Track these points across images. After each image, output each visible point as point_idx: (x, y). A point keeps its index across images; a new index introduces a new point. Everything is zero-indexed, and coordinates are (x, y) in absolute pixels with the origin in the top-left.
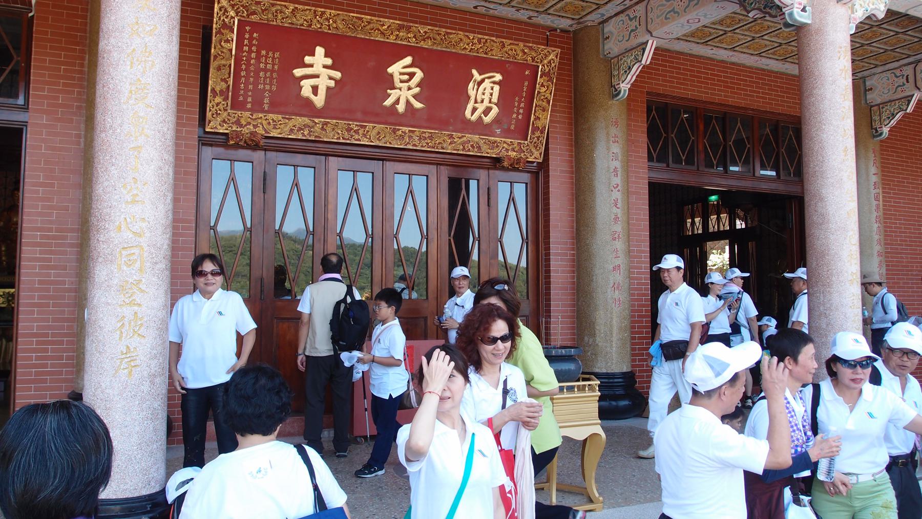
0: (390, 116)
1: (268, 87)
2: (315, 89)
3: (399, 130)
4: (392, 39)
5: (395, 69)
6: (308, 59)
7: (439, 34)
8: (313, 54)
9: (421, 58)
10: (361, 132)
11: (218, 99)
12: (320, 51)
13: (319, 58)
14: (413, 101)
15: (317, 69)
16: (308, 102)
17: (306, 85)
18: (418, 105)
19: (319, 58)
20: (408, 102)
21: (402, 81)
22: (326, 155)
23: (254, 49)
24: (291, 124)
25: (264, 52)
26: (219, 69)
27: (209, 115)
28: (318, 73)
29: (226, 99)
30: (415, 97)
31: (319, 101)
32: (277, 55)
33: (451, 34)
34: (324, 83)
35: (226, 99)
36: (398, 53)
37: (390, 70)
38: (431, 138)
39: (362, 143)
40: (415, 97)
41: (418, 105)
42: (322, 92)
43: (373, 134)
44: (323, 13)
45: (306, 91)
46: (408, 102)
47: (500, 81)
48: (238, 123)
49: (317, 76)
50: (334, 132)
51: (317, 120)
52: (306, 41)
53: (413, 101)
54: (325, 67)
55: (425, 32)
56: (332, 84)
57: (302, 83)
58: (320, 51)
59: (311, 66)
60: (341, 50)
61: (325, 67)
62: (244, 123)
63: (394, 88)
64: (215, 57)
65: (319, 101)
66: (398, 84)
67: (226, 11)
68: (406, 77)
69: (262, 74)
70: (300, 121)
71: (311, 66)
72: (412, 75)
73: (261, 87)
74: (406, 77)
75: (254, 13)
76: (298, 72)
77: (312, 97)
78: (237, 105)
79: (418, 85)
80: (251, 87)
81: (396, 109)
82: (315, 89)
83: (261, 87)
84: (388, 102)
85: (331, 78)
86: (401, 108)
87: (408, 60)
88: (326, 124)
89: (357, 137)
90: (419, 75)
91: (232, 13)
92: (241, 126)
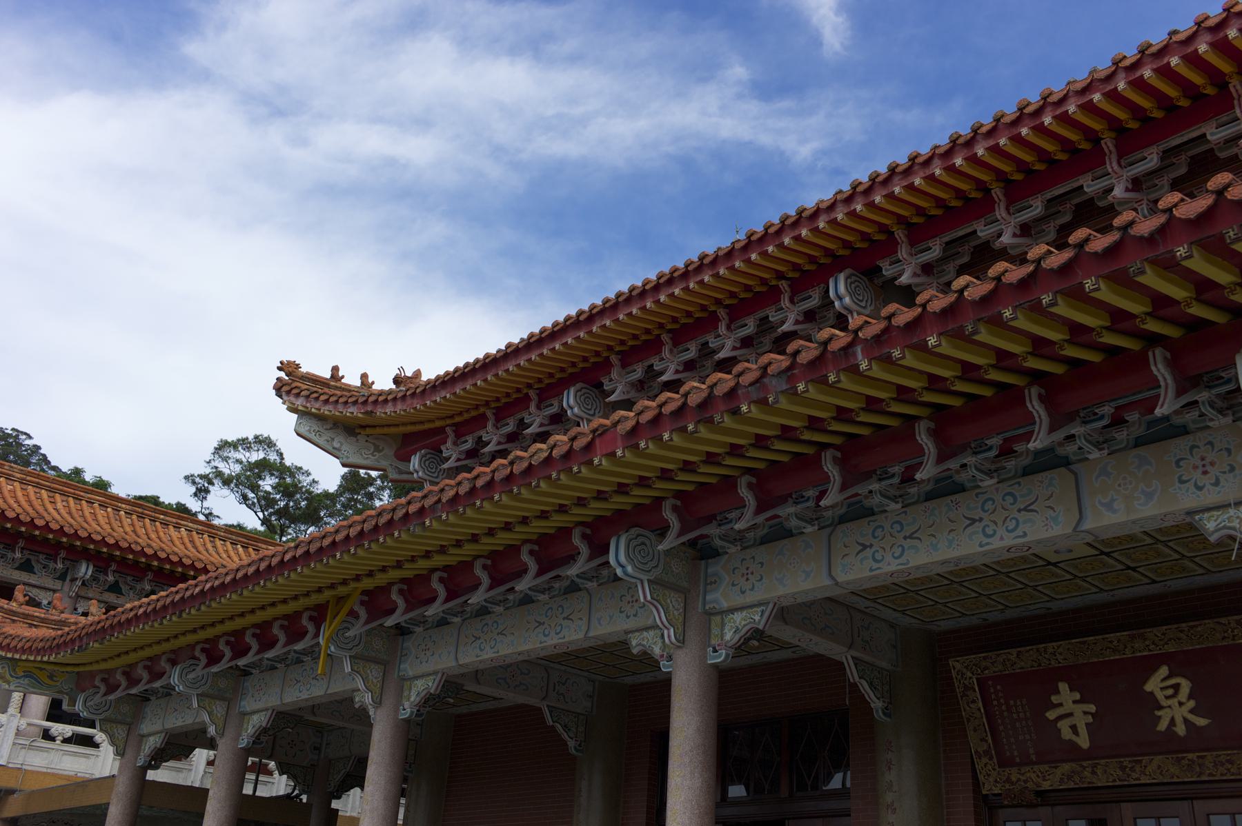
0: (1170, 744)
1: (1028, 737)
2: (1074, 728)
3: (1183, 758)
4: (1129, 654)
5: (1154, 685)
6: (1055, 699)
7: (1182, 631)
8: (1058, 692)
9: (1180, 663)
10: (1138, 768)
11: (985, 760)
12: (1063, 687)
13: (1066, 696)
14: (1191, 717)
15: (1069, 706)
16: (1073, 746)
17: (1064, 726)
18: (1201, 722)
19: (1066, 696)
20: (1186, 720)
21: (1167, 697)
22: (1192, 799)
23: (1002, 701)
24: (1059, 772)
25: (1012, 702)
26: (975, 730)
27: (981, 777)
28: (1073, 715)
29: (991, 759)
30: (1191, 711)
31: (1084, 741)
32: (1024, 701)
33: (1196, 626)
34: (1081, 722)
35: (991, 759)
36: (1148, 666)
37: (1149, 687)
38: (1231, 762)
39: (1142, 782)
40: (1191, 711)
41: (1201, 722)
42: (1083, 730)
43: (1155, 769)
44: (1045, 649)
45: (1066, 734)
46: (1186, 720)
47: (1048, 710)
48: (1008, 780)
49: (1071, 715)
50: (1105, 774)
51: (1085, 764)
52: (1047, 680)
53: (1191, 717)
54: (1074, 702)
55: (1164, 634)
56: (1090, 719)
57: (1059, 725)
58: (1063, 687)
59: (1061, 705)
60: (1085, 680)
61: (1074, 702)
62: (1014, 779)
63: (1161, 708)
64: (969, 720)
65: (1084, 741)
66: (1164, 703)
67: (963, 674)
68: (1170, 692)
69: (1018, 724)
70: (1066, 767)
71: (1061, 705)
72: (1176, 687)
73: (1021, 738)
74: (1170, 692)
75: (986, 668)
76: (1051, 715)
77: (1074, 738)
78: (1004, 763)
79: (1190, 697)
80: (1012, 740)
81: (1175, 733)
82: (1074, 728)
83: (1021, 738)
84: (1163, 726)
85: (1085, 713)
86: (1181, 730)
87: (1164, 671)
88: (1095, 766)
89: (1135, 775)
90: (1186, 686)
91: (969, 674)
92: (1012, 783)
